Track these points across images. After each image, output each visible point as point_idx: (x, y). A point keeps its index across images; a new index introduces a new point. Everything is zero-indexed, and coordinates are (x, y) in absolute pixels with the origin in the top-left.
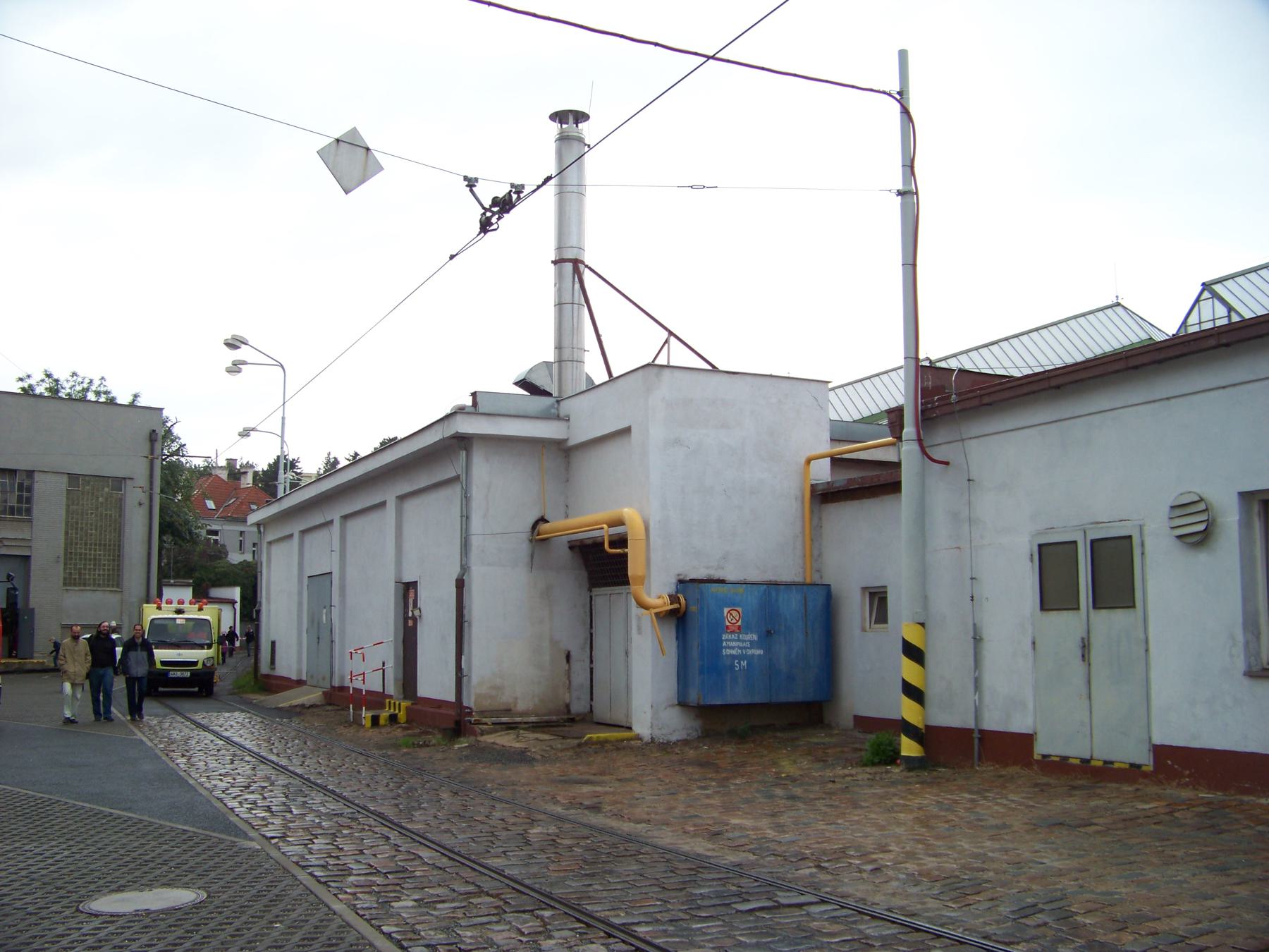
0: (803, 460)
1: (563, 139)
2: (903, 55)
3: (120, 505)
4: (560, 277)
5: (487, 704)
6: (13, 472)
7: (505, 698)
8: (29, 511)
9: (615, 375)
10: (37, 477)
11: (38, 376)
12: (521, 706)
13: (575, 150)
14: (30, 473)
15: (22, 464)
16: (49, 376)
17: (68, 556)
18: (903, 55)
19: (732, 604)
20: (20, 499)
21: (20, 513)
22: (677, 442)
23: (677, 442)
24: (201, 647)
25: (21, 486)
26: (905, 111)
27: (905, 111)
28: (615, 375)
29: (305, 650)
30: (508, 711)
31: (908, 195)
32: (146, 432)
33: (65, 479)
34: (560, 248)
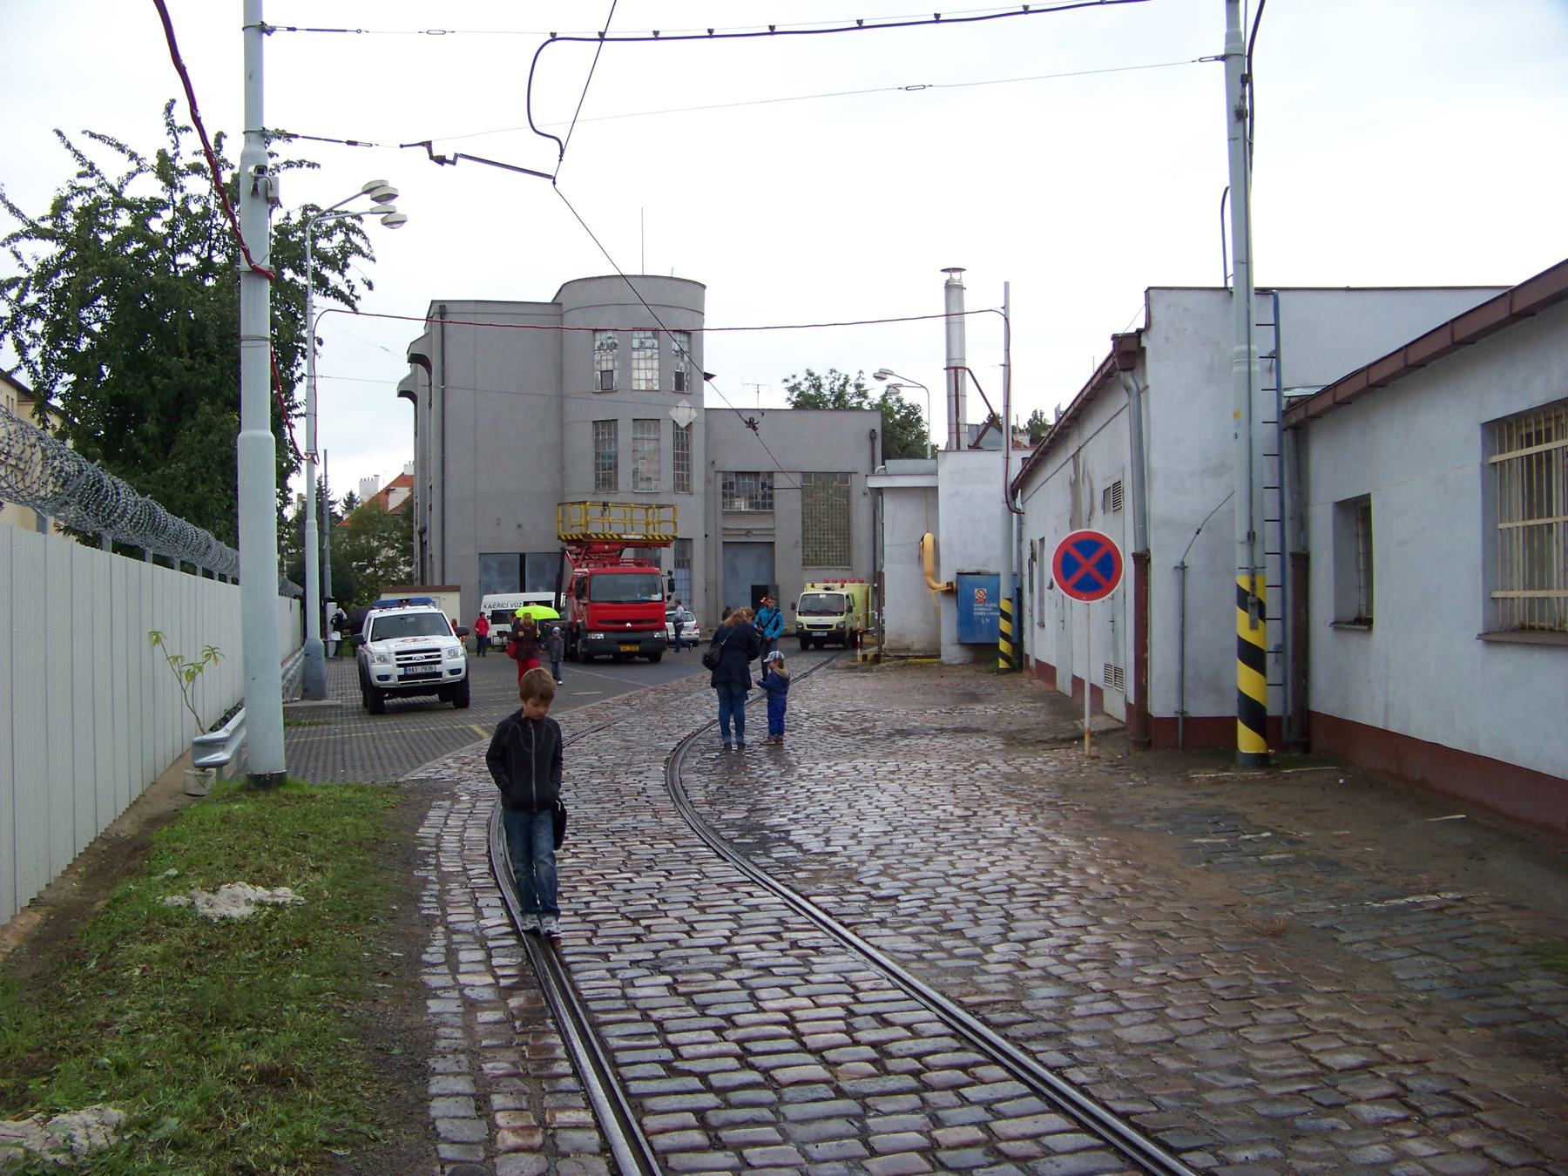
0: (998, 507)
1: (949, 286)
2: (1007, 285)
3: (847, 495)
4: (949, 376)
5: (894, 645)
6: (757, 474)
7: (906, 642)
8: (771, 506)
9: (448, 583)
10: (776, 476)
11: (801, 376)
12: (916, 647)
13: (955, 292)
14: (770, 474)
15: (764, 467)
16: (811, 374)
17: (805, 540)
18: (1007, 285)
19: (980, 586)
20: (764, 497)
21: (764, 506)
22: (957, 494)
23: (957, 494)
24: (835, 614)
25: (764, 485)
26: (1006, 319)
27: (1006, 319)
28: (448, 583)
30: (908, 649)
31: (1007, 366)
32: (866, 432)
33: (799, 476)
34: (948, 360)
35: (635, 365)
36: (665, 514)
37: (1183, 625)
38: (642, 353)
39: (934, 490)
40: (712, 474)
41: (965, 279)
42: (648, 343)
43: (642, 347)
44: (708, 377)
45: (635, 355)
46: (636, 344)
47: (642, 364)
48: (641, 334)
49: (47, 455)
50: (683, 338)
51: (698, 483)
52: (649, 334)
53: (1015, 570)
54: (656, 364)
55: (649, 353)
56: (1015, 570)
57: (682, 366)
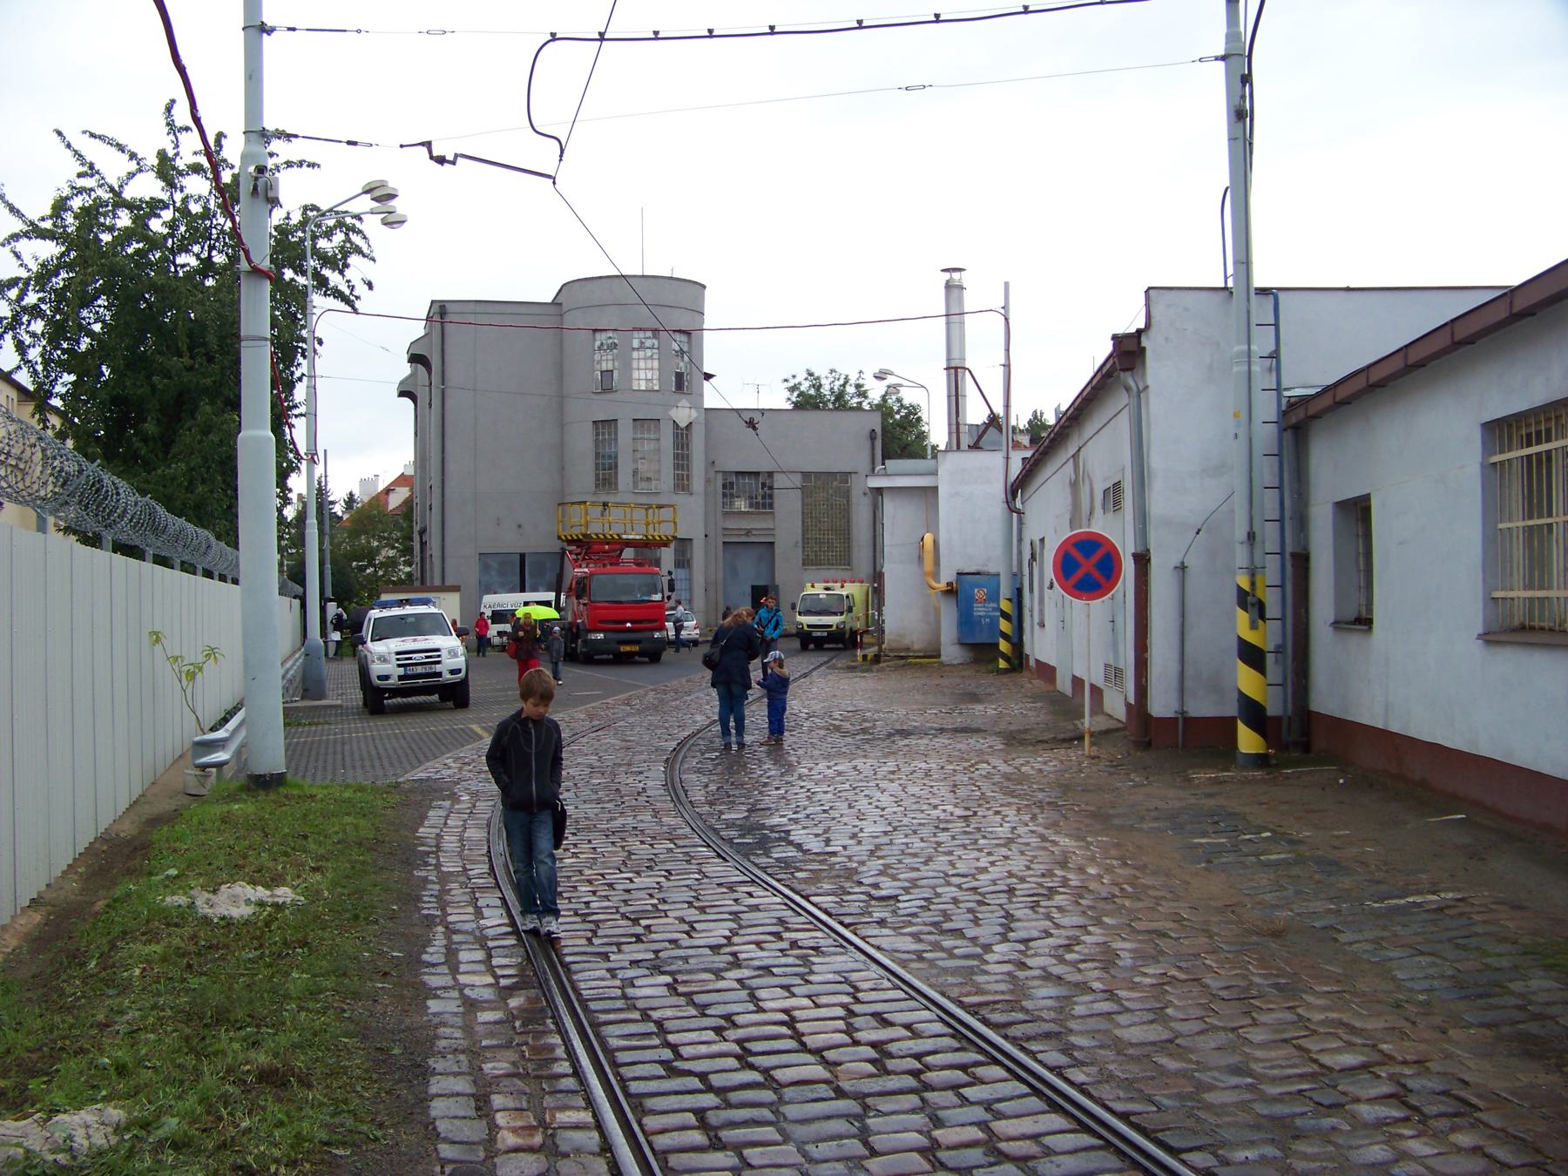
0: (998, 507)
1: (949, 286)
2: (1007, 285)
3: (847, 495)
4: (949, 376)
5: (894, 645)
6: (757, 474)
7: (906, 642)
8: (771, 506)
9: (448, 583)
10: (776, 476)
11: (801, 376)
12: (916, 647)
13: (955, 292)
14: (770, 474)
15: (764, 467)
16: (811, 374)
17: (805, 540)
18: (1007, 285)
19: (980, 586)
20: (764, 497)
21: (764, 506)
22: (957, 494)
23: (957, 494)
24: (835, 614)
25: (764, 485)
26: (1006, 319)
27: (1006, 319)
28: (448, 583)
29: (328, 572)
30: (908, 649)
31: (1007, 366)
32: (866, 432)
33: (799, 476)
34: (948, 360)
35: (635, 365)
36: (665, 514)
37: (1183, 625)
38: (642, 353)
39: (934, 490)
40: (712, 474)
41: (965, 279)
42: (648, 343)
43: (642, 347)
44: (708, 377)
45: (635, 355)
46: (636, 344)
47: (642, 364)
48: (641, 334)
49: (47, 455)
50: (683, 338)
51: (698, 483)
52: (649, 334)
53: (1015, 570)
54: (656, 364)
55: (649, 353)
56: (1015, 570)
57: (682, 366)
